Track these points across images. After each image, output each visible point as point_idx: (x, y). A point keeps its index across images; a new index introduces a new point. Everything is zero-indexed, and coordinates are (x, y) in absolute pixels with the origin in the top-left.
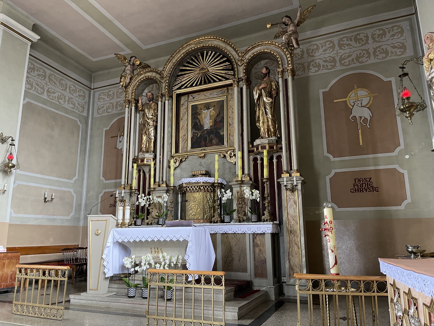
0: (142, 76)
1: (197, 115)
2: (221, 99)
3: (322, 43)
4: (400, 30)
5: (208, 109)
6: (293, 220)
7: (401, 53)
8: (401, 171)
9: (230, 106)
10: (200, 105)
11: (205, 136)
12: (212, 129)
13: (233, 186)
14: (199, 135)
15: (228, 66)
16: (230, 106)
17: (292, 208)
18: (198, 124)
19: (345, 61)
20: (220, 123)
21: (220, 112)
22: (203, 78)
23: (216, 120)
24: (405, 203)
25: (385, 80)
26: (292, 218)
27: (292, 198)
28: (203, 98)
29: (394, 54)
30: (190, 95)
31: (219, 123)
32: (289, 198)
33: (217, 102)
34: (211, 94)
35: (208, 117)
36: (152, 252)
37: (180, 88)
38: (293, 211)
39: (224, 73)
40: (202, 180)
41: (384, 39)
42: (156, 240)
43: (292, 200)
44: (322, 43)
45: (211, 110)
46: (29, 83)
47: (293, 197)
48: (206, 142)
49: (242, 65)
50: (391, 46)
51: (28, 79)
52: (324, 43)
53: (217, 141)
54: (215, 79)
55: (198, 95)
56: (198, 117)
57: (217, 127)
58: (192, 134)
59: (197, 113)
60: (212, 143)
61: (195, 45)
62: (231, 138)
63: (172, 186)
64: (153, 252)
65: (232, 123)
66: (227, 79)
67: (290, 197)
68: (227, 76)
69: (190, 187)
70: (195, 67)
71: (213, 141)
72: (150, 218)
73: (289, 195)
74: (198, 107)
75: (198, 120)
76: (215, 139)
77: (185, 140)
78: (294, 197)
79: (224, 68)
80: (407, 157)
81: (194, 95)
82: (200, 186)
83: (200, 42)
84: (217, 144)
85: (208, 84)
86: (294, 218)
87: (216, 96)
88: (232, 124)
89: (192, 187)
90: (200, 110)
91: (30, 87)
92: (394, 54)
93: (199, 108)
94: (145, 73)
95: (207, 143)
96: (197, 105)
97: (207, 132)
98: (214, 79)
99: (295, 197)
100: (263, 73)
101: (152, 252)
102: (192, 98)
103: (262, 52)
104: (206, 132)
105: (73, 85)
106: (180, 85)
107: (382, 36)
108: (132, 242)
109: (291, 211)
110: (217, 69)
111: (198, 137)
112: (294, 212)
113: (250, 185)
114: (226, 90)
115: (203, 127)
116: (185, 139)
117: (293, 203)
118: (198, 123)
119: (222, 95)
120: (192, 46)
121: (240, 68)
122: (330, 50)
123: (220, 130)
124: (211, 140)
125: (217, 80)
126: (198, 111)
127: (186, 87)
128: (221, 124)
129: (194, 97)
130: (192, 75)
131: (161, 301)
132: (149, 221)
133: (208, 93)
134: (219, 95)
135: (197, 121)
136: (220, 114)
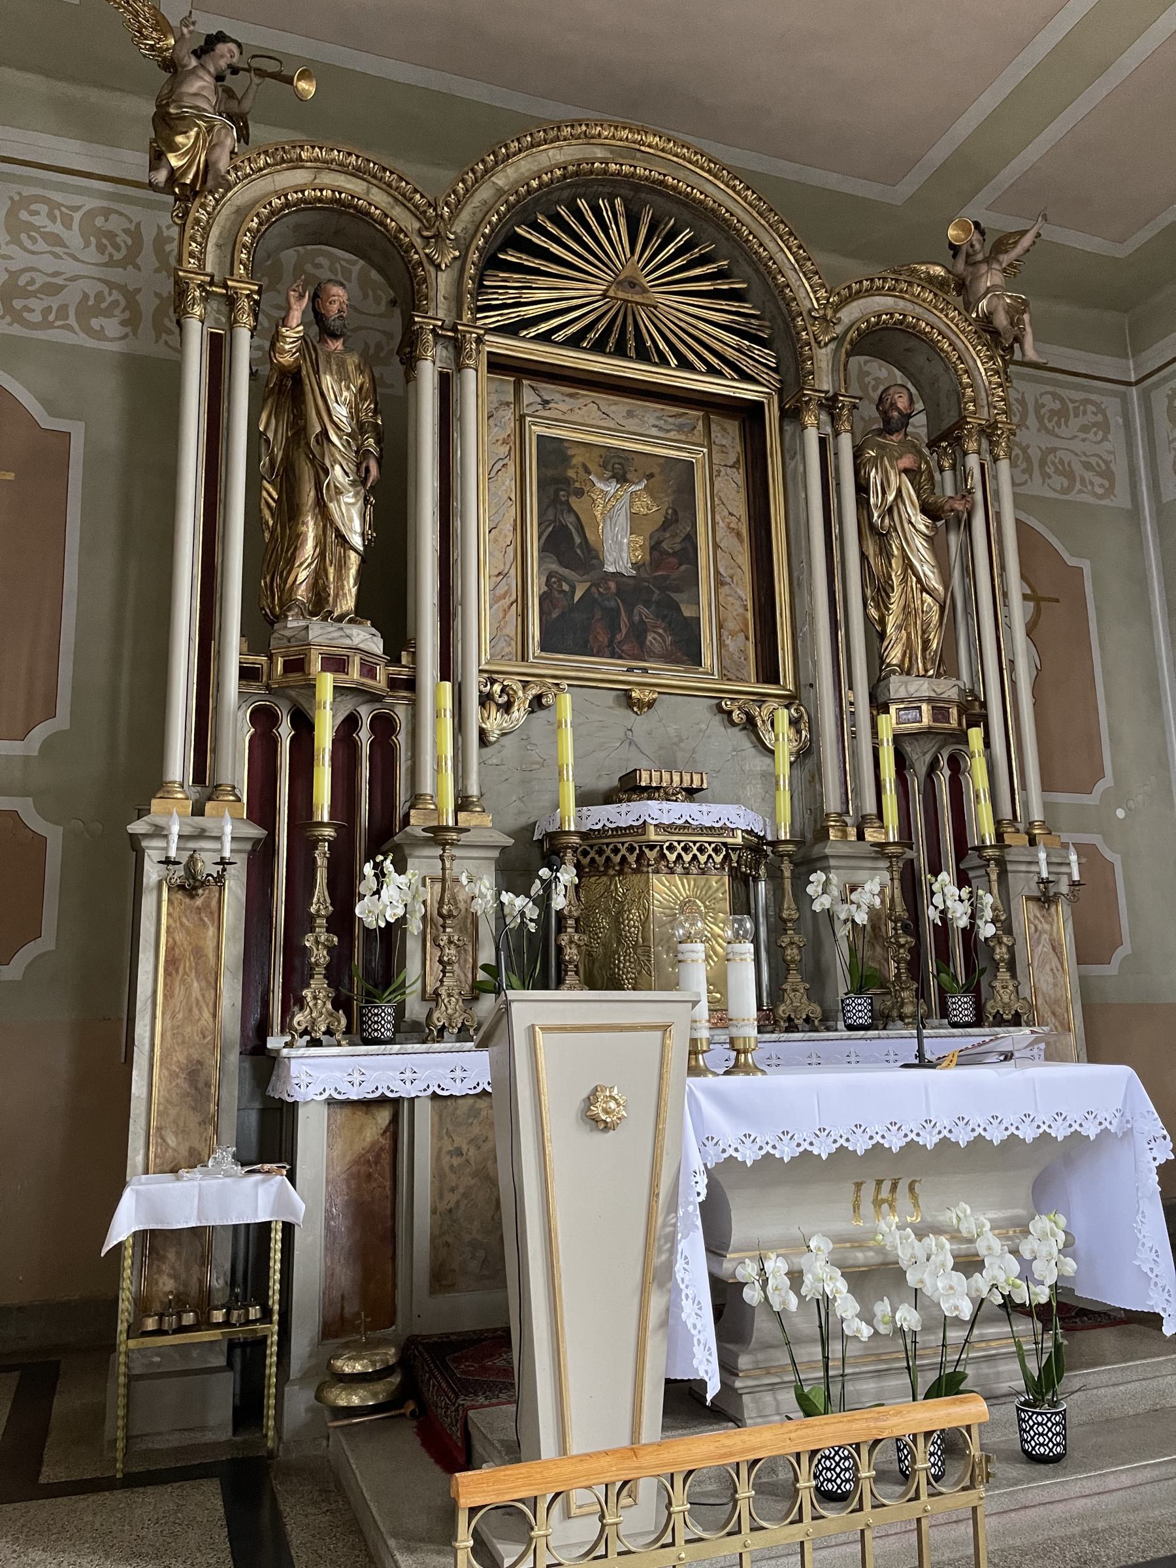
0: (300, 177)
1: (568, 495)
2: (683, 455)
3: (58, 327)
4: (1100, 418)
5: (622, 478)
6: (1054, 1013)
7: (33, 207)
8: (1108, 854)
9: (720, 499)
10: (583, 449)
11: (613, 604)
12: (644, 580)
13: (144, 844)
14: (578, 595)
15: (753, 321)
16: (720, 499)
17: (1048, 968)
18: (573, 539)
19: (32, 303)
20: (681, 565)
21: (675, 512)
22: (602, 325)
23: (659, 543)
24: (1120, 953)
25: (1071, 561)
26: (1050, 1006)
27: (1045, 932)
28: (592, 422)
29: (61, 213)
30: (525, 382)
31: (673, 560)
32: (1036, 929)
33: (662, 461)
34: (630, 414)
35: (622, 520)
36: (856, 1207)
37: (511, 330)
38: (1051, 980)
39: (733, 343)
40: (742, 820)
41: (1063, 431)
42: (929, 1140)
43: (1045, 937)
44: (58, 327)
45: (633, 488)
46: (104, 241)
47: (1047, 927)
48: (613, 636)
49: (826, 345)
50: (66, 250)
51: (111, 255)
52: (51, 326)
53: (669, 639)
54: (691, 357)
55: (567, 399)
56: (574, 502)
57: (666, 578)
58: (544, 579)
59: (568, 481)
60: (642, 644)
61: (612, 152)
62: (728, 642)
63: (572, 829)
64: (867, 1207)
65: (732, 577)
66: (745, 377)
67: (1039, 927)
68: (746, 365)
69: (623, 851)
70: (591, 258)
71: (649, 638)
72: (315, 998)
73: (1035, 917)
74: (570, 452)
75: (572, 518)
76: (661, 631)
77: (507, 601)
78: (1052, 925)
79: (733, 321)
80: (1120, 813)
81: (550, 390)
82: (640, 847)
83: (639, 155)
84: (669, 658)
85: (630, 359)
86: (1058, 1011)
87: (654, 432)
88: (728, 580)
89: (701, 850)
90: (581, 471)
91: (1066, 483)
92: (61, 213)
93: (574, 461)
94: (326, 165)
95: (619, 637)
96: (566, 445)
97: (618, 588)
98: (685, 357)
99: (1055, 928)
100: (898, 410)
101: (856, 1207)
102: (539, 400)
103: (909, 325)
104: (612, 585)
105: (1046, 393)
106: (514, 315)
107: (1060, 419)
108: (824, 1157)
109: (1042, 979)
110: (692, 310)
111: (576, 598)
112: (1055, 985)
113: (496, 854)
114: (700, 423)
115: (597, 557)
116: (506, 593)
117: (1048, 949)
118: (571, 533)
119: (683, 438)
120: (600, 153)
121: (823, 351)
122: (28, 284)
123: (681, 595)
124: (639, 632)
125: (673, 362)
126: (571, 473)
127: (545, 338)
128: (683, 568)
129: (547, 398)
130: (576, 291)
131: (1034, 1480)
132: (313, 1022)
133: (618, 406)
134: (668, 431)
135: (569, 520)
136: (677, 521)
